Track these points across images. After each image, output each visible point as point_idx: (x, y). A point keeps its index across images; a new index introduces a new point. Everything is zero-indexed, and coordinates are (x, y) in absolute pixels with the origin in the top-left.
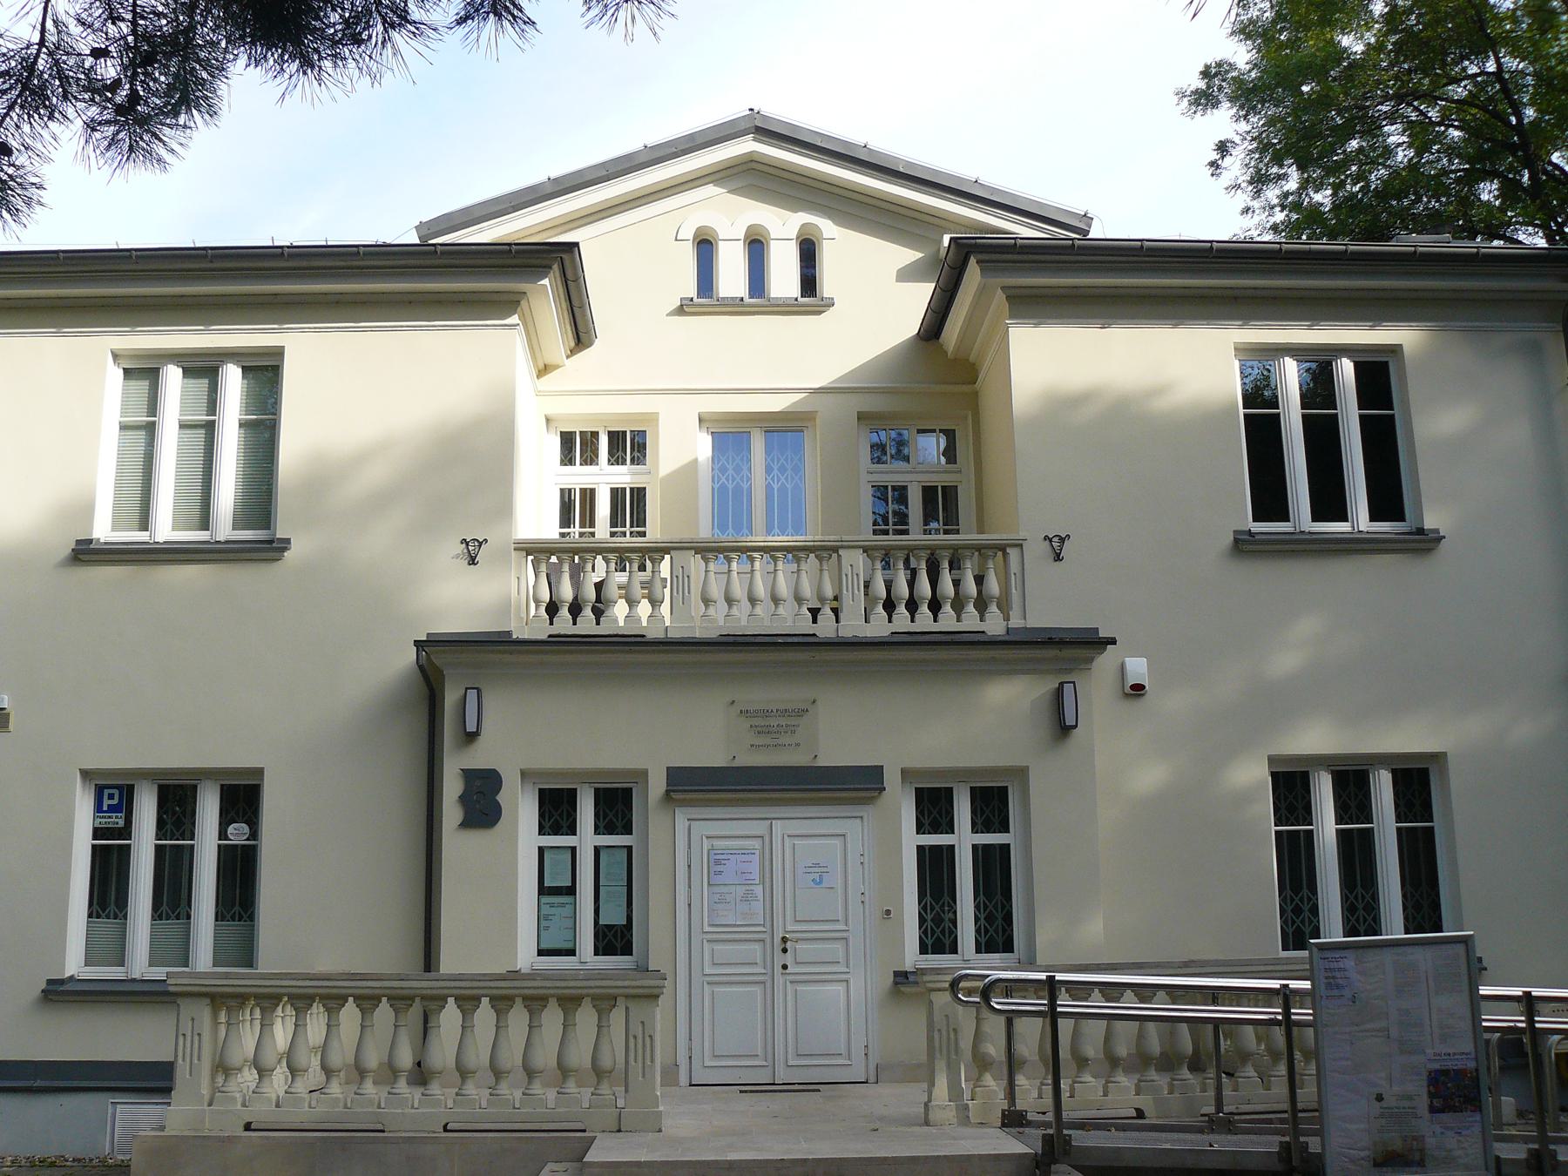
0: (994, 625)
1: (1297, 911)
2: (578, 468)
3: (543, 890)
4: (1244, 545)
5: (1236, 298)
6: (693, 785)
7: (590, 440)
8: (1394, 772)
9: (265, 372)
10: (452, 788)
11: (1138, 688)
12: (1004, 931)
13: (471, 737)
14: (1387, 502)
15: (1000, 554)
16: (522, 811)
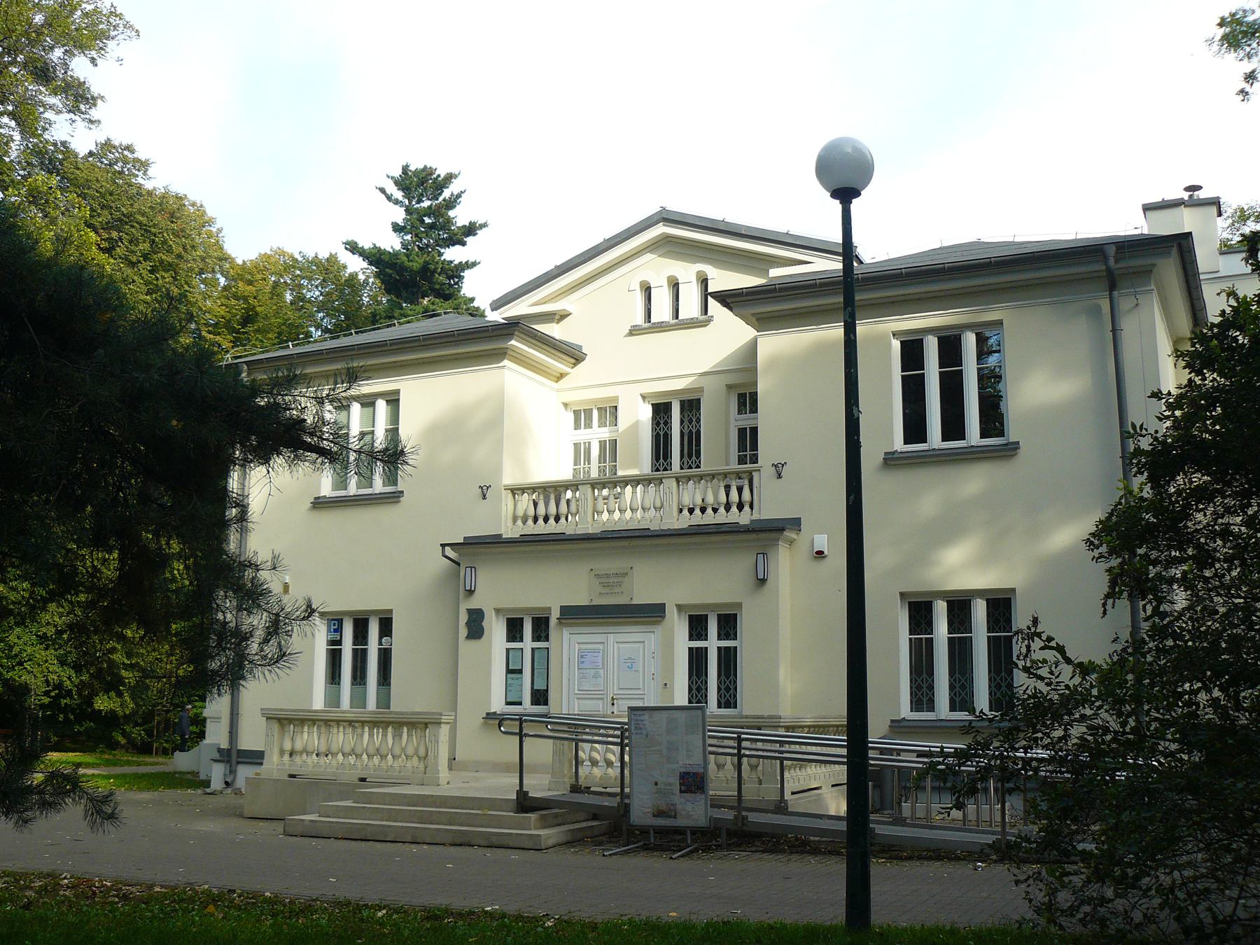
0: (744, 518)
1: (963, 687)
3: (509, 671)
6: (573, 614)
7: (588, 413)
8: (988, 600)
9: (393, 400)
10: (464, 618)
11: (820, 553)
13: (471, 592)
16: (496, 631)
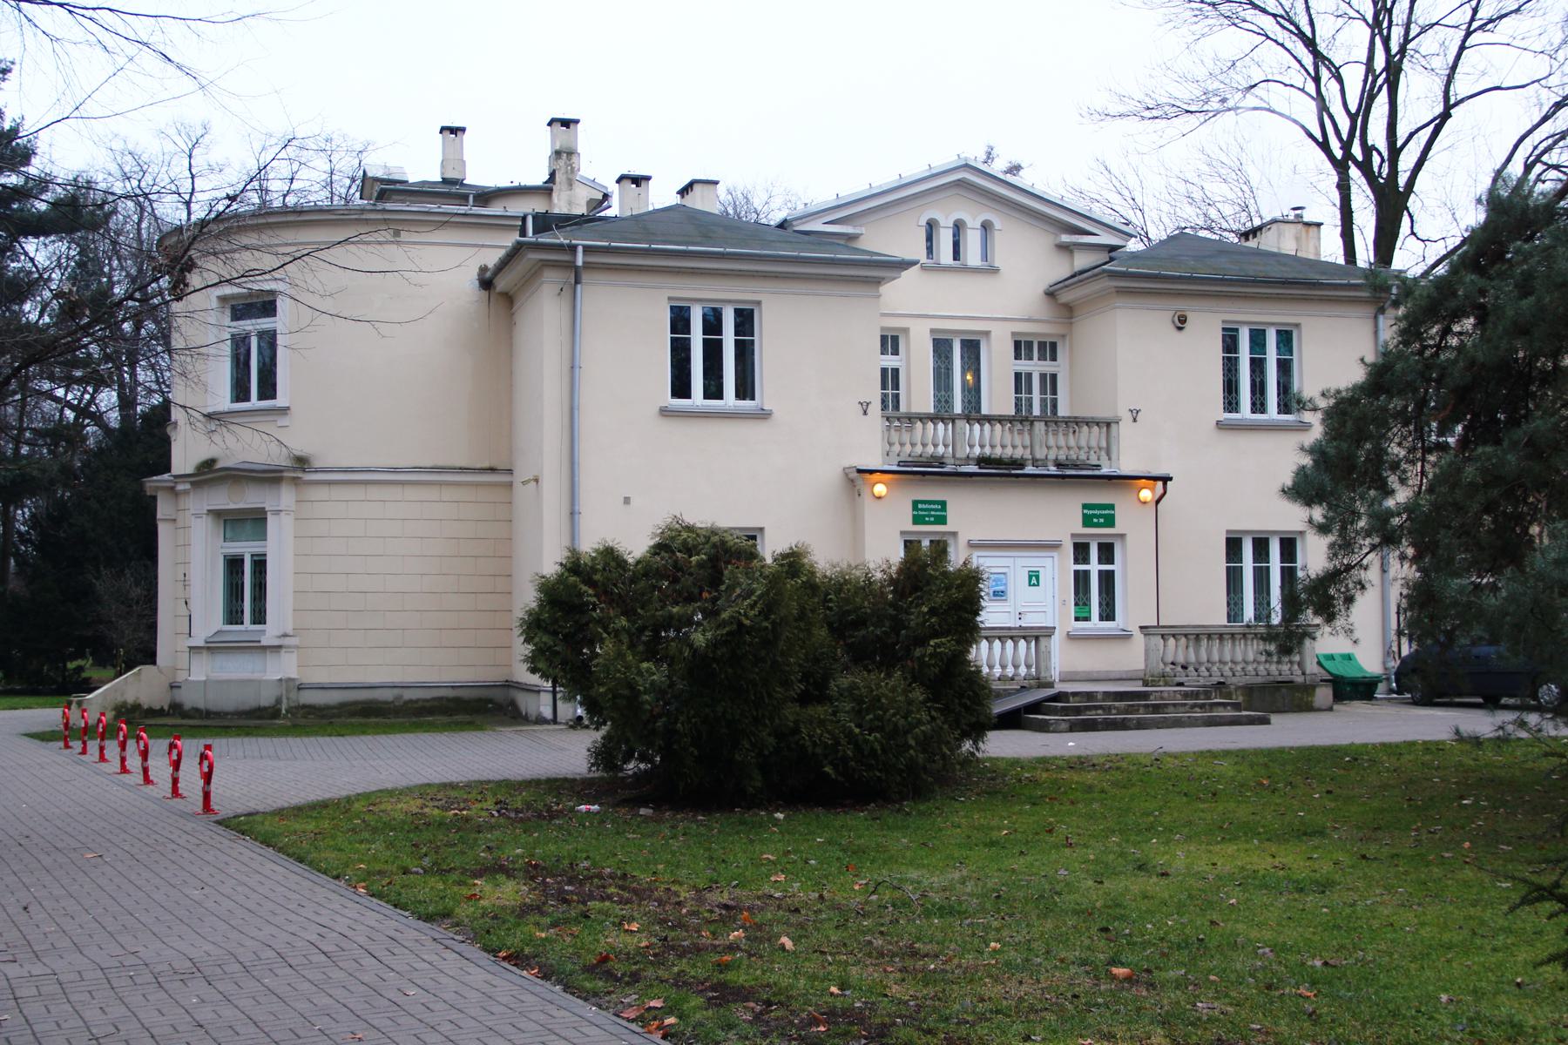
2: (1023, 362)
4: (665, 412)
7: (1029, 345)
10: (250, 498)
14: (745, 389)
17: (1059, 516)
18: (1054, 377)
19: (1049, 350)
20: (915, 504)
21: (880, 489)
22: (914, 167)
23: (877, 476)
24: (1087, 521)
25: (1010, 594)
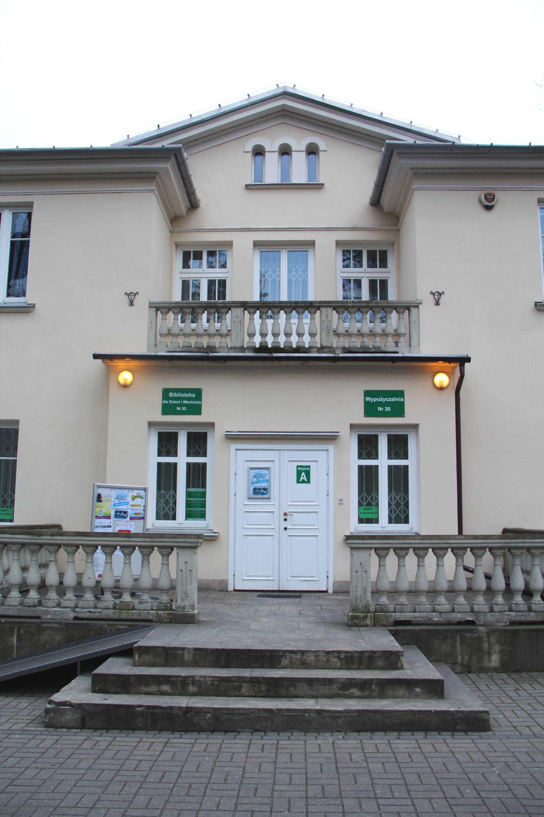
2: (352, 269)
5: (50, 179)
7: (358, 255)
12: (405, 512)
15: (407, 311)
17: (340, 405)
18: (384, 283)
19: (378, 258)
20: (166, 392)
21: (126, 377)
22: (232, 95)
23: (120, 363)
24: (370, 410)
25: (274, 492)
